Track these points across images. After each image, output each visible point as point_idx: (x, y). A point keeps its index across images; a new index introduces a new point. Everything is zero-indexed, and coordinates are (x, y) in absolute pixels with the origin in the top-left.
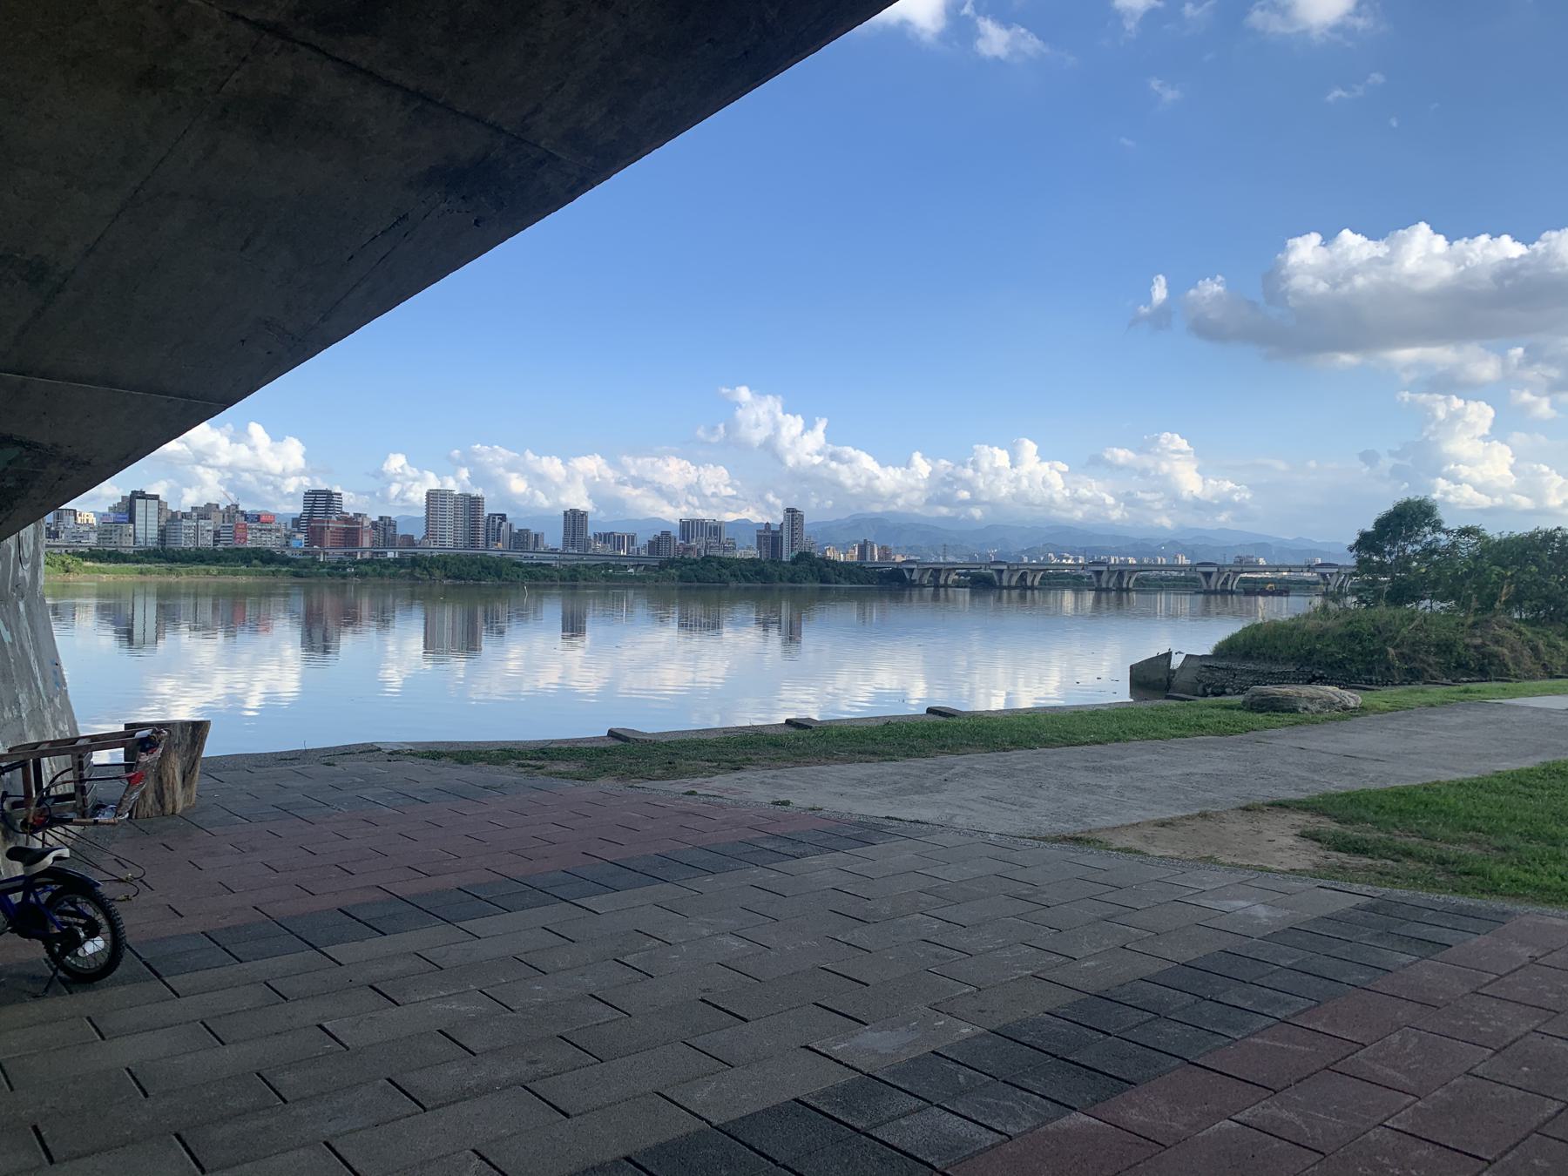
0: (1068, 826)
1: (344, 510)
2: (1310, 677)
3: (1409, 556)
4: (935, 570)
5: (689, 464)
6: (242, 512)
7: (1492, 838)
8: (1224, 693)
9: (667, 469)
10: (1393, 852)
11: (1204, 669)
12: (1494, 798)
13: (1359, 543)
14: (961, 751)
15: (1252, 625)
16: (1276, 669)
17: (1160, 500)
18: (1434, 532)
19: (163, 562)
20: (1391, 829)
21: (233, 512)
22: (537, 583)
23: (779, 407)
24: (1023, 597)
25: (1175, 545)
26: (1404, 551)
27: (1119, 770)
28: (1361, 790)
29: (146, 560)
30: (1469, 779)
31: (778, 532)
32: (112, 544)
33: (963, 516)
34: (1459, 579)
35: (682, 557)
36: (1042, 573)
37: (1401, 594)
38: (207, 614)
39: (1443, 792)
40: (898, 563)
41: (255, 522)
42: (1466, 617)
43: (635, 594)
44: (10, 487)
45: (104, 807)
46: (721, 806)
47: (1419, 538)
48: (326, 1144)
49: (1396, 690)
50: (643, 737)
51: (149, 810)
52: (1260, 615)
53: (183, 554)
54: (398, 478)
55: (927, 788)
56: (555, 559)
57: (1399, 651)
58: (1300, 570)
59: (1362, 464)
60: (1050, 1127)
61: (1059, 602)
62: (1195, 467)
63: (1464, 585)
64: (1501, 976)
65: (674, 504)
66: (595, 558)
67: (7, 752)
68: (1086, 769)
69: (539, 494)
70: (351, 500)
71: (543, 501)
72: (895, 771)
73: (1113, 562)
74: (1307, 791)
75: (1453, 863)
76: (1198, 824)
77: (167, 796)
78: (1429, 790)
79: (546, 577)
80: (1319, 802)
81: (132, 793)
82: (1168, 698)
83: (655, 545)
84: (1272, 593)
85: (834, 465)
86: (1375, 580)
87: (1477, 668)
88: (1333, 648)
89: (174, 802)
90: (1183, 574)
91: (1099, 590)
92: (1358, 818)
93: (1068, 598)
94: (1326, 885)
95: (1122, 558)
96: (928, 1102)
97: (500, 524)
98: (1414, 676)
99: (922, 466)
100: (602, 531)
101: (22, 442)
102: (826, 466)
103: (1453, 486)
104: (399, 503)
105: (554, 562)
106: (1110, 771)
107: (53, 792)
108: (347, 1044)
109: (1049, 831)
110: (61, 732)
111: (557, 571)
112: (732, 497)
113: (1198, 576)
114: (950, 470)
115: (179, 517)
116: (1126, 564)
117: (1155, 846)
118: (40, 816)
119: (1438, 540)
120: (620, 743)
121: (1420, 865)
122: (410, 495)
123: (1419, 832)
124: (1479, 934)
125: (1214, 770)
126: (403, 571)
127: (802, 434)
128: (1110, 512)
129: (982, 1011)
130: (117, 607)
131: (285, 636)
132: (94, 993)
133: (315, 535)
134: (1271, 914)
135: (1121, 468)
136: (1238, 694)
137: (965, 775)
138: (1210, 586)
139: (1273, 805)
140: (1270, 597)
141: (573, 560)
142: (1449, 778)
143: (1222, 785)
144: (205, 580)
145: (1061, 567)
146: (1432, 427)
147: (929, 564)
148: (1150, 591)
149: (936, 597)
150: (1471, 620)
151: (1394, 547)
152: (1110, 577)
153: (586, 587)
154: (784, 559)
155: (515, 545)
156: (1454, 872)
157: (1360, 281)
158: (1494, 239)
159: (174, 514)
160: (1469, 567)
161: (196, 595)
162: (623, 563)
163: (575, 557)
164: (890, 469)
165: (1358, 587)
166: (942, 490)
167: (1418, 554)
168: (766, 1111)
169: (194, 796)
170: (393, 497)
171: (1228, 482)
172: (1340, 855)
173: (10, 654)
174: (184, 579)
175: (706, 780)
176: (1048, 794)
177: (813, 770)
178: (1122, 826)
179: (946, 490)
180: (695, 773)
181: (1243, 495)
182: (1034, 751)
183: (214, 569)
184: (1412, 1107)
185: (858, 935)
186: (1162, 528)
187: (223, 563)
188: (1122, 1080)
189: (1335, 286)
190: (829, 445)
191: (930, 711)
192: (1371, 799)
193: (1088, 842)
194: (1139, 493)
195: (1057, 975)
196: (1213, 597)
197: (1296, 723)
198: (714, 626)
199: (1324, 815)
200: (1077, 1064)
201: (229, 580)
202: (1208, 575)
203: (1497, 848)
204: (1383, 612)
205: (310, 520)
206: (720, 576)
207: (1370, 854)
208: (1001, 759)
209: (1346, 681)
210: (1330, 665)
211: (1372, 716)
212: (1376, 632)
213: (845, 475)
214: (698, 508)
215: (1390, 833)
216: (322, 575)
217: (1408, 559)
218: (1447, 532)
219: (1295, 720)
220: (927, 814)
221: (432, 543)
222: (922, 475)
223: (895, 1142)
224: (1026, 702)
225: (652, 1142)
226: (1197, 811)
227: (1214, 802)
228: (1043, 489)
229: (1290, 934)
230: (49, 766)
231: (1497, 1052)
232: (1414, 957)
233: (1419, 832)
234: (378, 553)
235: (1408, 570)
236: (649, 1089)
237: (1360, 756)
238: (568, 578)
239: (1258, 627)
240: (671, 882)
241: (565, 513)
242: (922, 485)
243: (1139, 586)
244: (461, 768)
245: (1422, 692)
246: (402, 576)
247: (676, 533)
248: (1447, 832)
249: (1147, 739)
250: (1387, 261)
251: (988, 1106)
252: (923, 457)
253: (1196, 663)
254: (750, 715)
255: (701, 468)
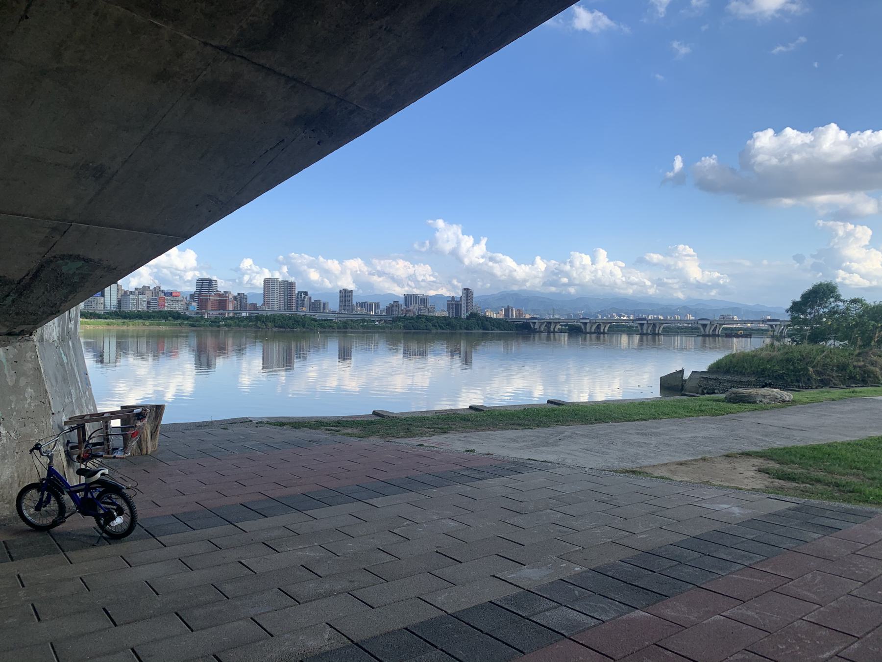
0: (628, 465)
1: (218, 289)
2: (764, 384)
3: (821, 315)
4: (548, 323)
5: (409, 263)
6: (162, 291)
7: (866, 473)
8: (714, 393)
9: (397, 266)
10: (809, 479)
11: (702, 379)
12: (868, 451)
13: (792, 308)
14: (567, 424)
15: (730, 355)
16: (744, 379)
17: (677, 283)
18: (836, 301)
19: (120, 319)
20: (809, 468)
21: (157, 291)
22: (325, 330)
23: (460, 231)
24: (598, 338)
25: (686, 309)
26: (818, 312)
27: (656, 435)
28: (792, 446)
29: (111, 317)
30: (854, 441)
31: (459, 301)
32: (92, 309)
33: (564, 292)
34: (850, 328)
35: (405, 316)
36: (609, 324)
37: (816, 337)
38: (143, 348)
39: (839, 448)
40: (527, 319)
41: (170, 296)
42: (854, 350)
43: (379, 336)
44: (76, 282)
45: (117, 449)
46: (437, 452)
47: (827, 305)
48: (252, 618)
49: (812, 391)
50: (392, 415)
51: (134, 452)
52: (735, 348)
53: (131, 314)
54: (249, 272)
55: (550, 444)
56: (335, 317)
57: (815, 369)
58: (758, 323)
59: (794, 262)
60: (624, 617)
61: (619, 341)
62: (697, 264)
63: (853, 332)
64: (869, 545)
65: (401, 286)
66: (357, 316)
67: (68, 420)
68: (638, 434)
69: (326, 280)
70: (222, 284)
71: (328, 284)
72: (531, 434)
73: (650, 318)
74: (762, 446)
75: (844, 486)
76: (701, 463)
77: (143, 445)
78: (831, 447)
79: (330, 327)
80: (768, 452)
81: (132, 442)
82: (683, 395)
83: (390, 309)
84: (742, 336)
85: (491, 264)
86: (802, 328)
87: (861, 379)
88: (777, 368)
89: (147, 447)
90: (690, 325)
91: (642, 334)
92: (791, 462)
93: (624, 339)
94: (772, 497)
95: (655, 316)
96: (559, 604)
97: (304, 297)
98: (824, 383)
99: (541, 265)
100: (361, 301)
101: (83, 258)
102: (486, 264)
103: (848, 274)
104: (249, 286)
105: (334, 318)
106: (651, 435)
107: (90, 442)
108: (256, 571)
109: (618, 467)
110: (90, 410)
111: (336, 323)
112: (433, 282)
113: (699, 326)
114: (557, 266)
115: (128, 294)
116: (658, 319)
117: (677, 475)
118: (86, 453)
119: (838, 306)
120: (379, 418)
121: (825, 487)
122: (254, 281)
123: (825, 469)
124: (856, 523)
125: (709, 435)
126: (251, 323)
127: (473, 246)
128: (648, 290)
129: (586, 560)
130: (95, 343)
131: (186, 359)
132: (122, 544)
133: (202, 304)
134: (742, 512)
135: (655, 265)
136: (722, 393)
137: (570, 437)
138: (706, 332)
139: (743, 454)
140: (741, 338)
141: (344, 317)
142: (843, 440)
143: (714, 443)
144: (143, 328)
145: (620, 321)
146: (836, 240)
147: (545, 319)
148: (671, 335)
149: (548, 339)
150: (857, 351)
151: (812, 309)
152: (648, 327)
153: (352, 333)
154: (462, 317)
155: (312, 309)
156: (844, 491)
157: (796, 157)
158: (875, 132)
159: (125, 292)
160: (856, 322)
161: (137, 337)
162: (372, 319)
163: (346, 316)
164: (523, 266)
165: (791, 332)
166: (552, 278)
167: (826, 314)
168: (475, 607)
169: (157, 445)
170: (246, 282)
171: (716, 273)
172: (780, 481)
173: (67, 369)
174: (131, 328)
175: (429, 438)
176: (617, 447)
177: (486, 433)
178: (659, 465)
179: (554, 277)
180: (422, 435)
181: (724, 280)
182: (608, 424)
183: (147, 322)
184: (818, 610)
185: (519, 520)
186: (679, 299)
187: (152, 319)
188: (662, 595)
189: (781, 160)
190: (488, 252)
191: (549, 402)
192: (798, 451)
193: (640, 473)
194: (665, 280)
195: (624, 541)
196: (707, 338)
197: (756, 409)
198: (423, 354)
199: (771, 460)
200: (638, 586)
201: (155, 328)
202: (704, 326)
203: (869, 479)
204: (806, 347)
205: (200, 295)
206: (426, 326)
207: (797, 481)
208: (590, 428)
209: (784, 386)
210: (775, 377)
211: (799, 406)
212: (802, 359)
213: (497, 270)
214: (414, 288)
215: (808, 470)
216: (207, 326)
217: (821, 317)
218: (843, 301)
219: (755, 407)
220: (551, 458)
221: (267, 308)
222: (540, 269)
223: (544, 623)
224: (600, 397)
225: (417, 621)
226: (700, 457)
227: (710, 452)
228: (610, 277)
229: (751, 523)
230: (89, 428)
231: (865, 584)
232: (820, 535)
233: (825, 469)
234: (237, 313)
235: (821, 323)
236: (413, 595)
237: (791, 427)
238: (342, 327)
239: (733, 356)
240: (415, 492)
241: (340, 291)
242: (541, 275)
243: (665, 332)
244: (295, 431)
245: (828, 392)
246: (250, 326)
247: (402, 302)
248: (840, 469)
249: (671, 418)
250: (812, 145)
251: (591, 606)
252: (541, 259)
253: (698, 376)
254: (444, 405)
255: (416, 266)
